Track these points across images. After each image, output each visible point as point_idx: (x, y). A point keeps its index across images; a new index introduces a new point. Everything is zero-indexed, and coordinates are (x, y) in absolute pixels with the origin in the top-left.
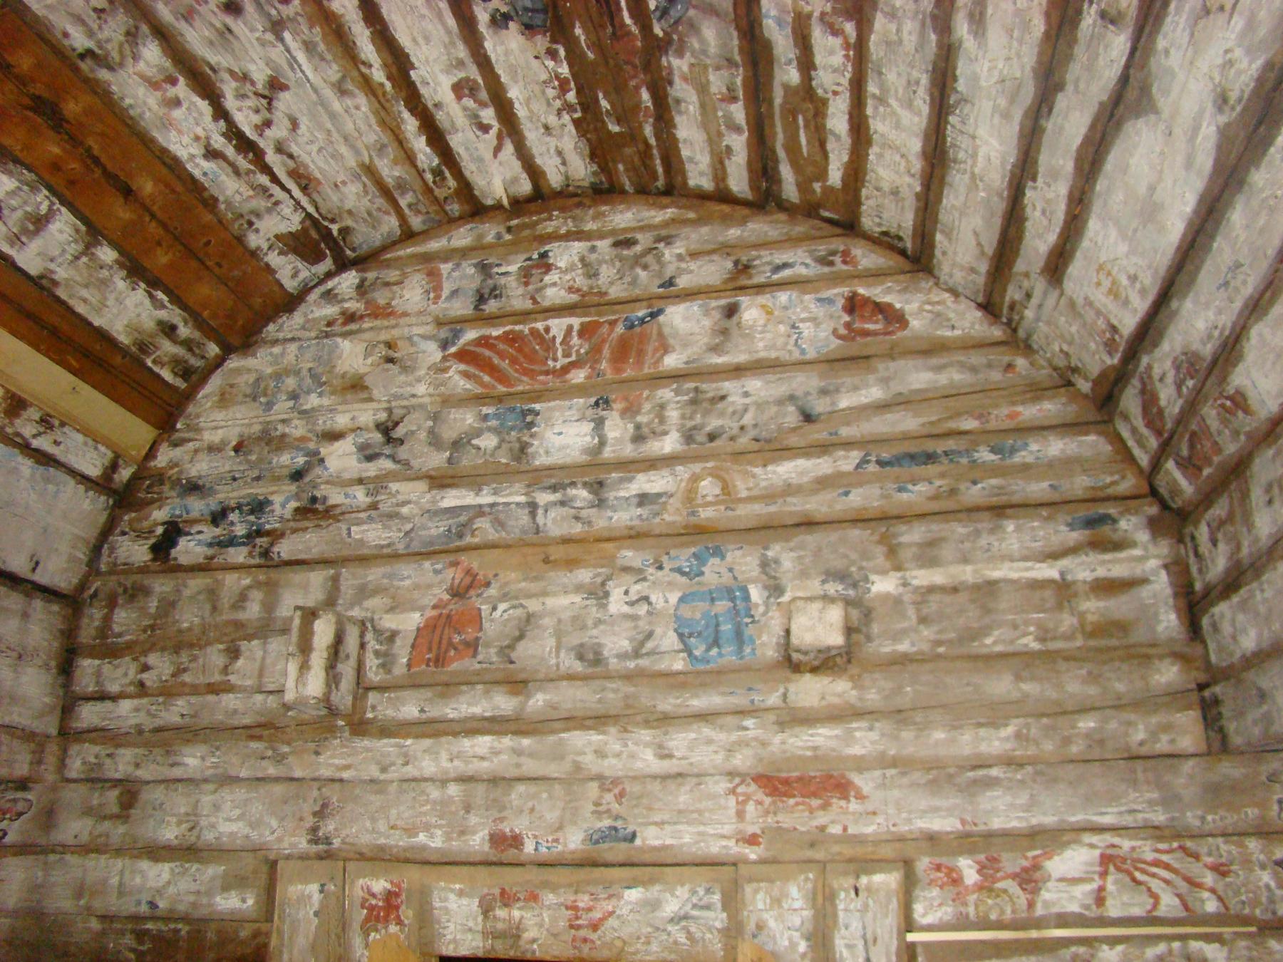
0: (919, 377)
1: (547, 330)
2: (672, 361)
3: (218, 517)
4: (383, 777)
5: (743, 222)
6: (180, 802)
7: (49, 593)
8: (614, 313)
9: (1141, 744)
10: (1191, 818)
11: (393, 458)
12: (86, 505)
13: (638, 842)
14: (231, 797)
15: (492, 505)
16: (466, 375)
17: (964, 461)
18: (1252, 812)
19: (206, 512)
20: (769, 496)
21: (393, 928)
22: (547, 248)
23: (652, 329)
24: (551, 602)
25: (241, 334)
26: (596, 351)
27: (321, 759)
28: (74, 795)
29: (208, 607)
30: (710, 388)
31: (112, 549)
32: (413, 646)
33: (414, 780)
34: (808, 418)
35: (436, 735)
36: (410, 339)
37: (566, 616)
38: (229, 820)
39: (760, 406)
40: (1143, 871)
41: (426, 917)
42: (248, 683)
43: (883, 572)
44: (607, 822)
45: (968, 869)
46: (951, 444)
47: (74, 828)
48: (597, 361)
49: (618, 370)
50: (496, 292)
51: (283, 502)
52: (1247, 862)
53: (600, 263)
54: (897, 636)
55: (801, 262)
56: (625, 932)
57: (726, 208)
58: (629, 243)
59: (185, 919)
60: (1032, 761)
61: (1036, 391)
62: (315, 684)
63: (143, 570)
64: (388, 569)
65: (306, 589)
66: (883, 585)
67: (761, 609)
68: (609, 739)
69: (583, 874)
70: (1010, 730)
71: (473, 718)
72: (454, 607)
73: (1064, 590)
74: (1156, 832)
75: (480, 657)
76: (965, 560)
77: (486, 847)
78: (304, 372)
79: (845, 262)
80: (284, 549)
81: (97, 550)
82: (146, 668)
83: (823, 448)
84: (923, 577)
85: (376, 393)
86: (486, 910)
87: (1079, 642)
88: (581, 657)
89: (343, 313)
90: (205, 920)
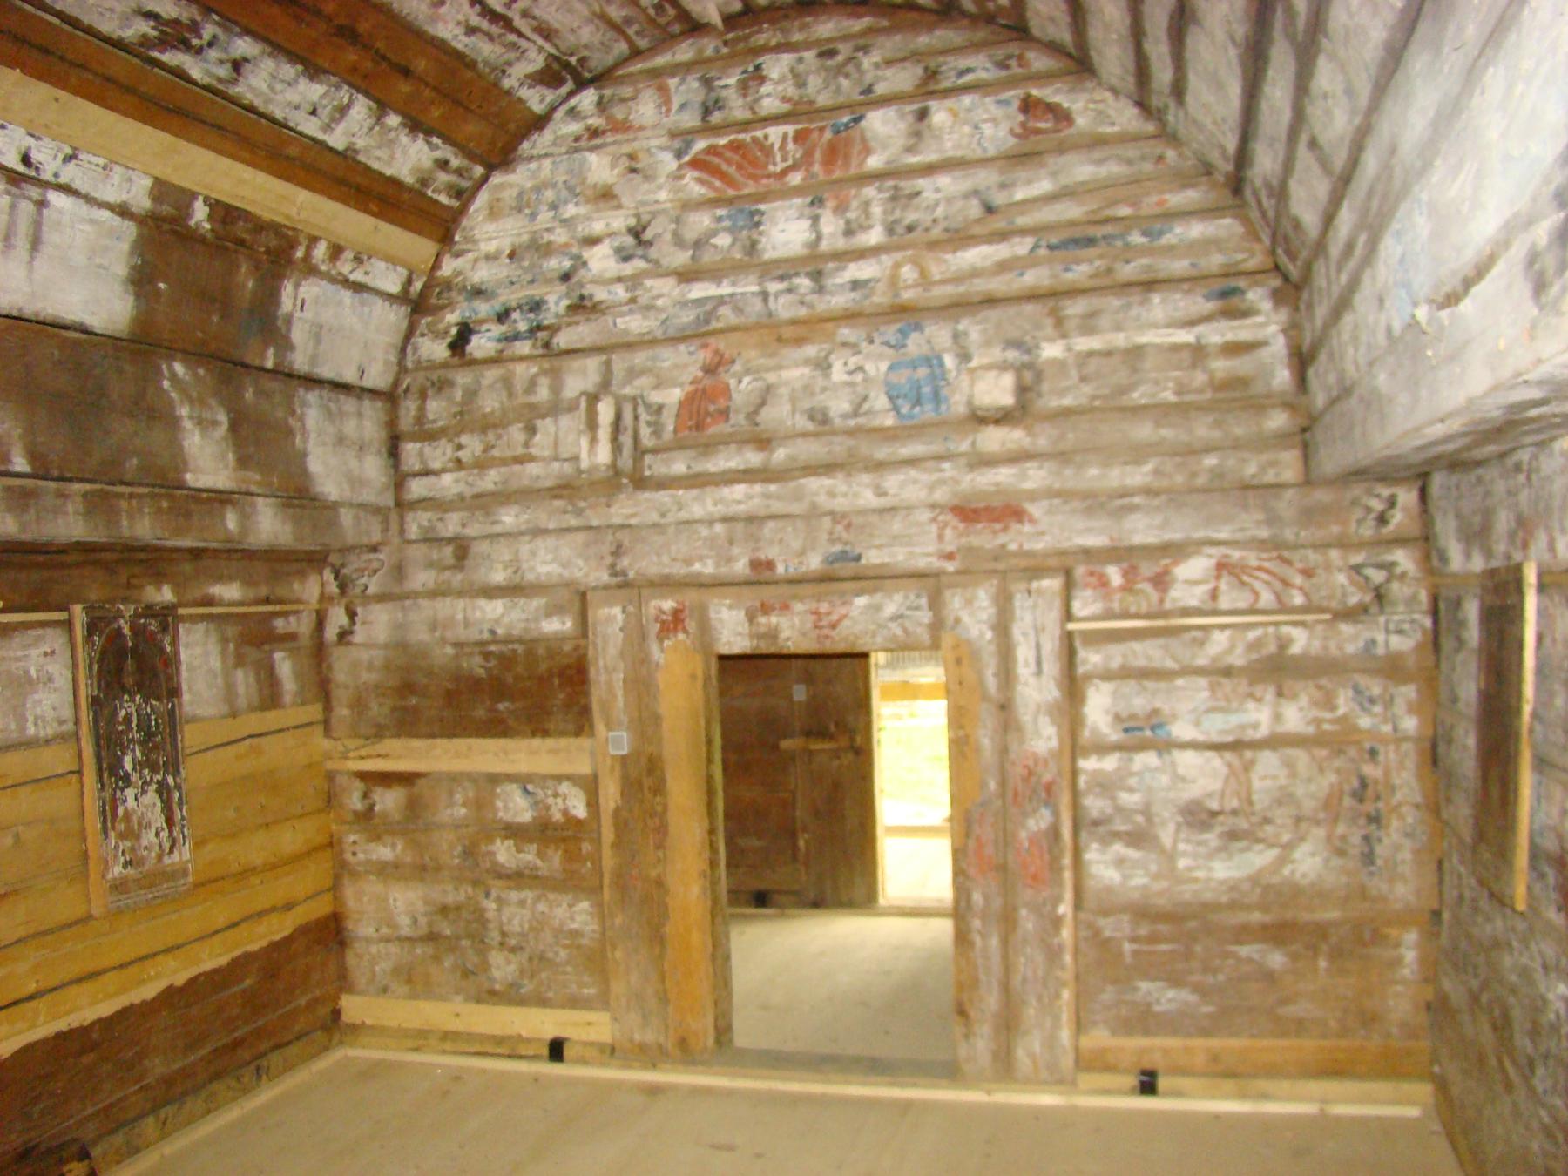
0: (1082, 170)
1: (766, 137)
2: (874, 162)
3: (503, 316)
4: (663, 521)
5: (931, 28)
6: (503, 552)
7: (374, 393)
8: (823, 119)
9: (1253, 476)
10: (1289, 534)
11: (645, 258)
12: (392, 317)
13: (863, 561)
14: (543, 545)
15: (732, 295)
16: (700, 181)
17: (1119, 243)
18: (1335, 529)
19: (492, 313)
20: (957, 279)
21: (681, 636)
22: (761, 60)
23: (854, 133)
24: (786, 374)
25: (501, 157)
26: (808, 155)
27: (612, 510)
28: (417, 552)
29: (504, 394)
30: (907, 185)
31: (415, 349)
32: (677, 416)
33: (688, 522)
34: (990, 210)
35: (703, 485)
36: (648, 150)
37: (798, 385)
38: (545, 562)
39: (949, 201)
40: (1251, 576)
41: (705, 627)
42: (546, 453)
43: (1051, 340)
44: (838, 548)
45: (1114, 575)
46: (1108, 229)
47: (421, 579)
48: (811, 164)
49: (828, 172)
50: (718, 104)
51: (557, 302)
52: (1328, 567)
53: (808, 73)
54: (1062, 393)
55: (981, 67)
56: (857, 629)
57: (914, 15)
58: (831, 53)
59: (520, 641)
60: (1168, 491)
61: (1184, 180)
62: (603, 454)
63: (445, 365)
64: (650, 352)
65: (580, 378)
66: (1051, 351)
67: (954, 373)
68: (836, 482)
69: (823, 587)
70: (1148, 467)
71: (730, 471)
72: (708, 382)
73: (1198, 352)
74: (1262, 545)
75: (732, 422)
76: (1118, 328)
77: (747, 571)
78: (560, 185)
79: (1020, 66)
80: (562, 340)
81: (403, 350)
82: (460, 447)
83: (1002, 236)
84: (1083, 344)
85: (625, 200)
86: (751, 618)
87: (1208, 395)
88: (812, 418)
89: (588, 128)
90: (535, 641)
